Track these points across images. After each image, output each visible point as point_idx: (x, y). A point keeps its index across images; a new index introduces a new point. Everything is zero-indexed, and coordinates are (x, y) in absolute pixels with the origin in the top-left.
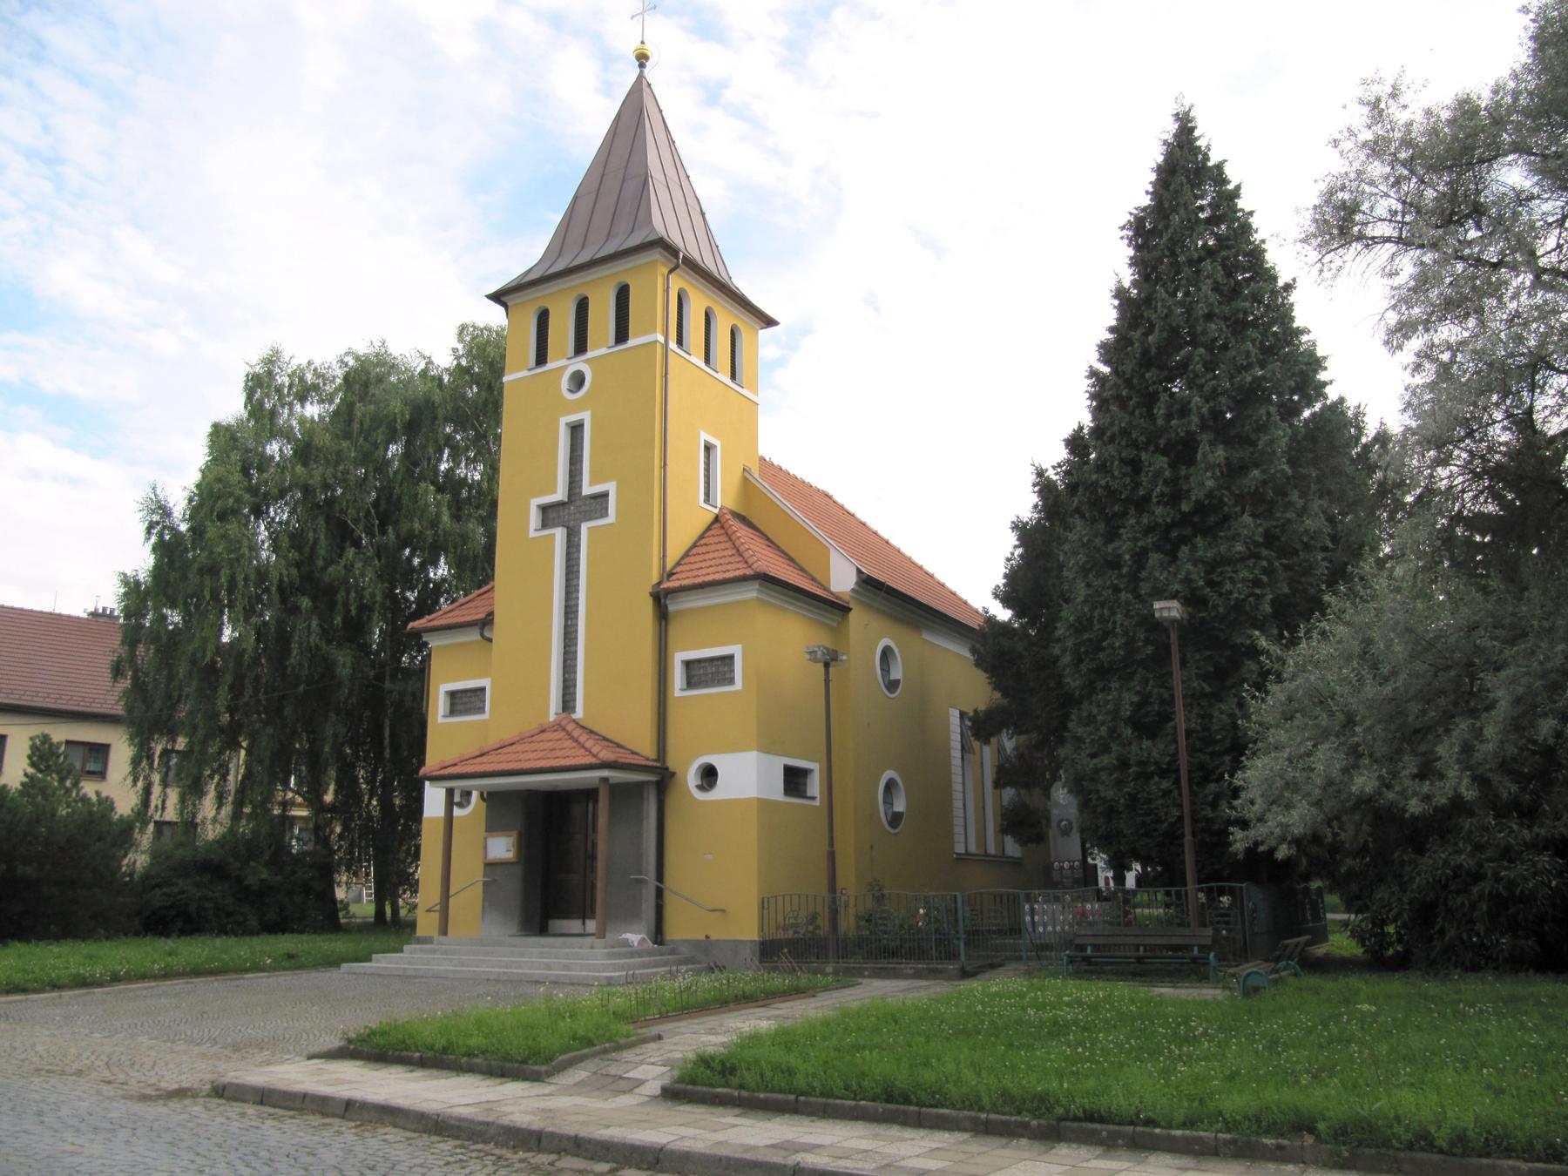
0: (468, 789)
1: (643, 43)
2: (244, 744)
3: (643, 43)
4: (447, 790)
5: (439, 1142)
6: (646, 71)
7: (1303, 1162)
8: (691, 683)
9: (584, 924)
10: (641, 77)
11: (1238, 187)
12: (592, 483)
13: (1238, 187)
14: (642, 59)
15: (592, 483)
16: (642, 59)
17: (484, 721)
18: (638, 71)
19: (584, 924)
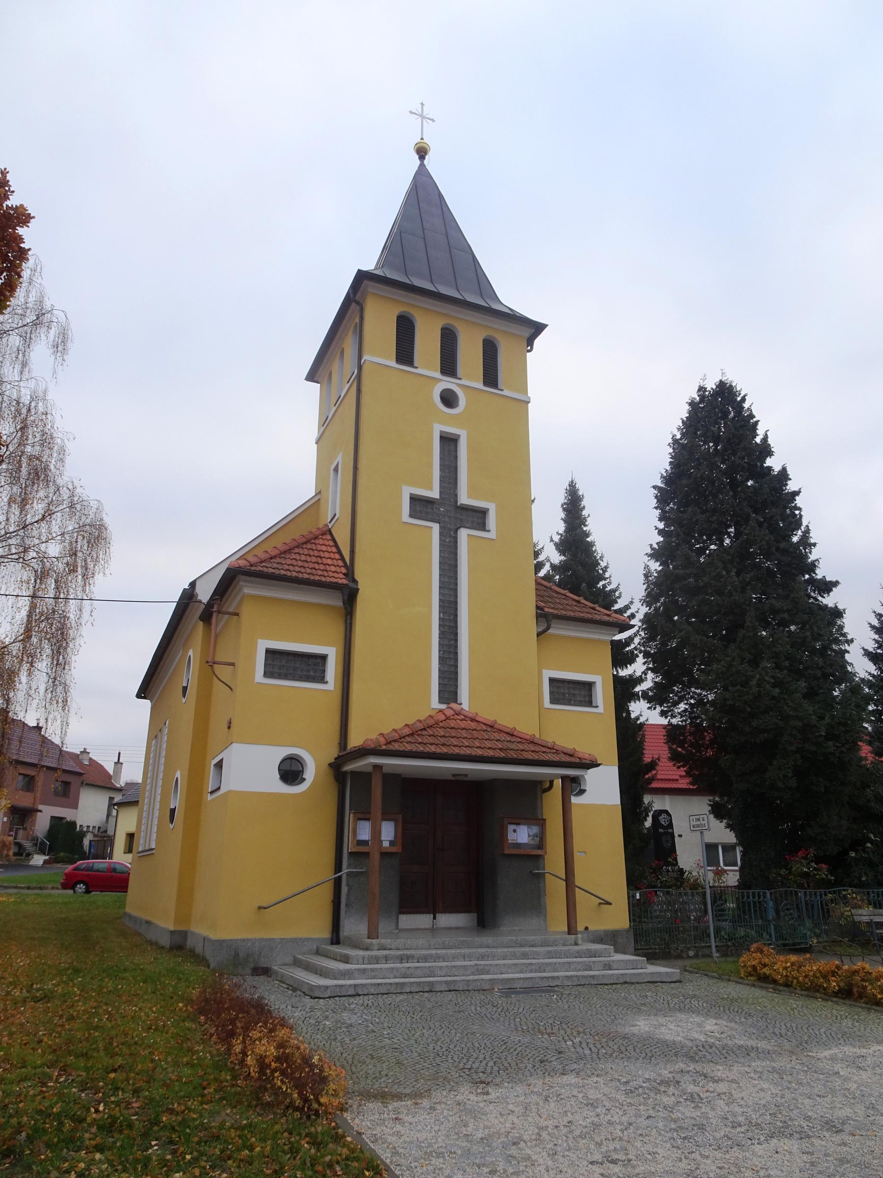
0: (355, 842)
1: (422, 139)
2: (865, 751)
3: (422, 139)
4: (402, 912)
5: (28, 292)
6: (426, 162)
7: (61, 751)
8: (589, 686)
9: (434, 918)
10: (422, 165)
11: (784, 470)
12: (431, 488)
13: (784, 470)
14: (422, 152)
15: (431, 488)
16: (422, 152)
17: (549, 668)
18: (418, 162)
19: (434, 918)
